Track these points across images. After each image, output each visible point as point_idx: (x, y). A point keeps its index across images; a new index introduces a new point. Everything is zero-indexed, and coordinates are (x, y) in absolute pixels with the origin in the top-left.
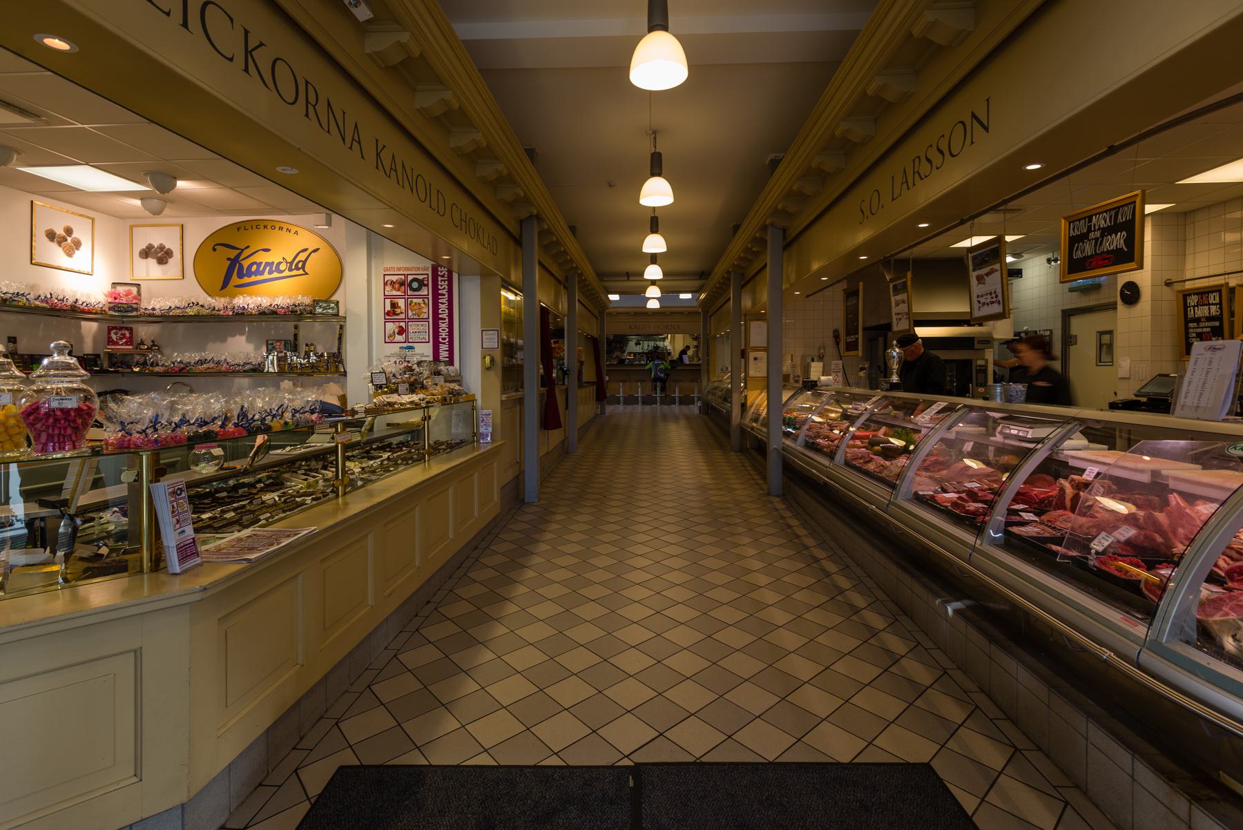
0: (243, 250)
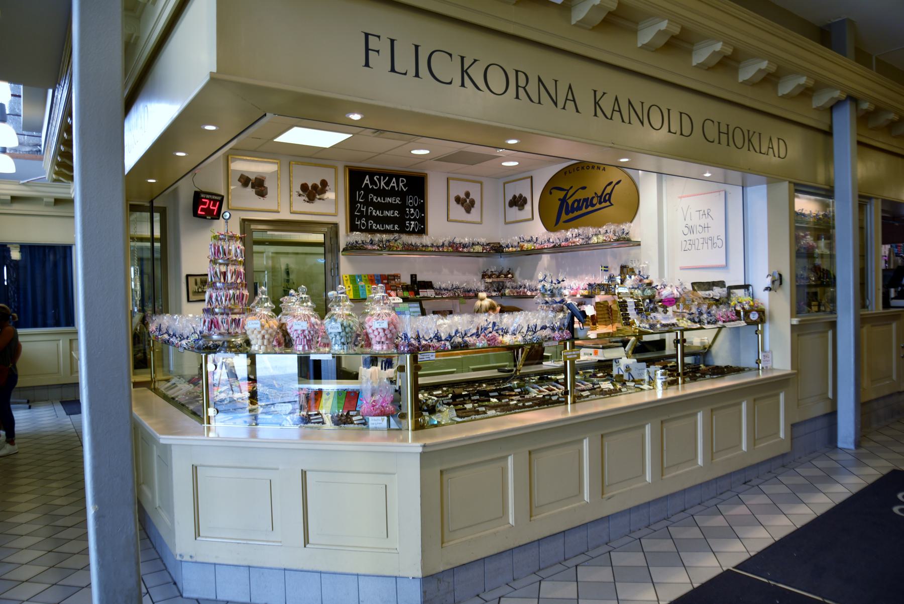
0: (568, 191)
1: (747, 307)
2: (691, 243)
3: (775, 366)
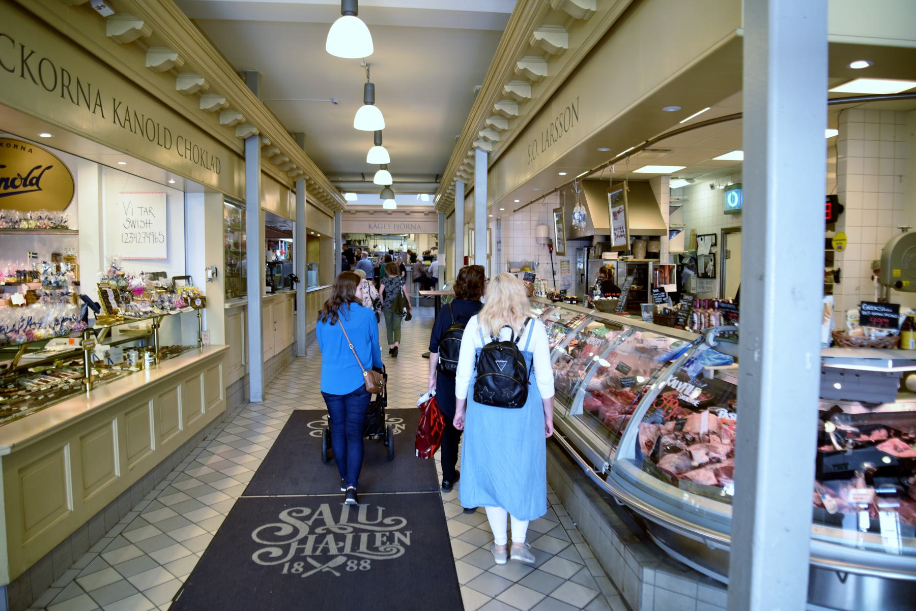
1: (191, 294)
2: (133, 236)
3: (212, 343)
